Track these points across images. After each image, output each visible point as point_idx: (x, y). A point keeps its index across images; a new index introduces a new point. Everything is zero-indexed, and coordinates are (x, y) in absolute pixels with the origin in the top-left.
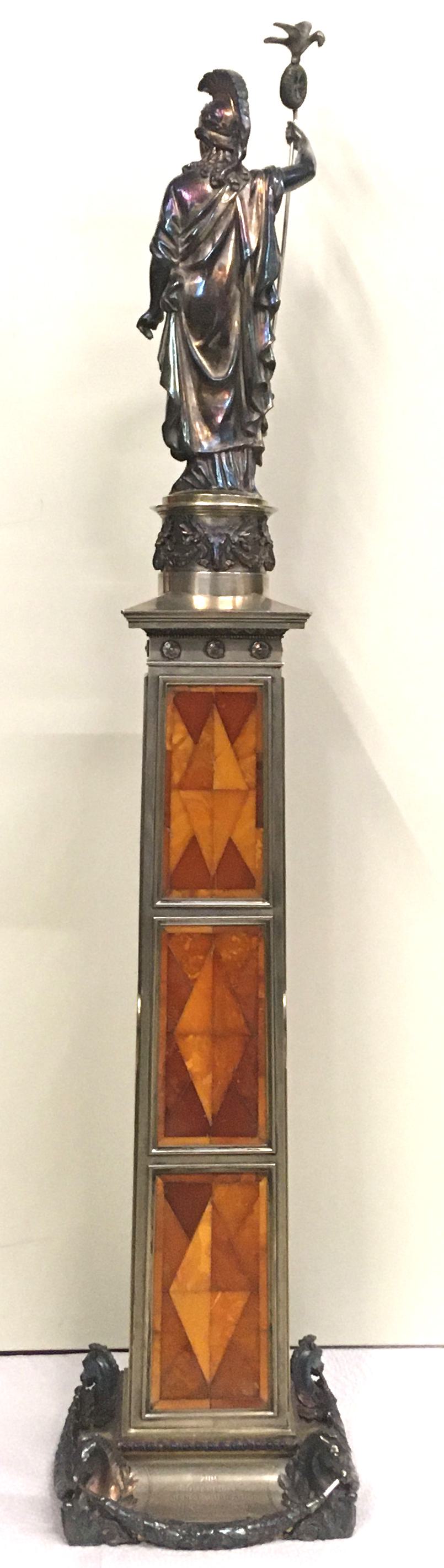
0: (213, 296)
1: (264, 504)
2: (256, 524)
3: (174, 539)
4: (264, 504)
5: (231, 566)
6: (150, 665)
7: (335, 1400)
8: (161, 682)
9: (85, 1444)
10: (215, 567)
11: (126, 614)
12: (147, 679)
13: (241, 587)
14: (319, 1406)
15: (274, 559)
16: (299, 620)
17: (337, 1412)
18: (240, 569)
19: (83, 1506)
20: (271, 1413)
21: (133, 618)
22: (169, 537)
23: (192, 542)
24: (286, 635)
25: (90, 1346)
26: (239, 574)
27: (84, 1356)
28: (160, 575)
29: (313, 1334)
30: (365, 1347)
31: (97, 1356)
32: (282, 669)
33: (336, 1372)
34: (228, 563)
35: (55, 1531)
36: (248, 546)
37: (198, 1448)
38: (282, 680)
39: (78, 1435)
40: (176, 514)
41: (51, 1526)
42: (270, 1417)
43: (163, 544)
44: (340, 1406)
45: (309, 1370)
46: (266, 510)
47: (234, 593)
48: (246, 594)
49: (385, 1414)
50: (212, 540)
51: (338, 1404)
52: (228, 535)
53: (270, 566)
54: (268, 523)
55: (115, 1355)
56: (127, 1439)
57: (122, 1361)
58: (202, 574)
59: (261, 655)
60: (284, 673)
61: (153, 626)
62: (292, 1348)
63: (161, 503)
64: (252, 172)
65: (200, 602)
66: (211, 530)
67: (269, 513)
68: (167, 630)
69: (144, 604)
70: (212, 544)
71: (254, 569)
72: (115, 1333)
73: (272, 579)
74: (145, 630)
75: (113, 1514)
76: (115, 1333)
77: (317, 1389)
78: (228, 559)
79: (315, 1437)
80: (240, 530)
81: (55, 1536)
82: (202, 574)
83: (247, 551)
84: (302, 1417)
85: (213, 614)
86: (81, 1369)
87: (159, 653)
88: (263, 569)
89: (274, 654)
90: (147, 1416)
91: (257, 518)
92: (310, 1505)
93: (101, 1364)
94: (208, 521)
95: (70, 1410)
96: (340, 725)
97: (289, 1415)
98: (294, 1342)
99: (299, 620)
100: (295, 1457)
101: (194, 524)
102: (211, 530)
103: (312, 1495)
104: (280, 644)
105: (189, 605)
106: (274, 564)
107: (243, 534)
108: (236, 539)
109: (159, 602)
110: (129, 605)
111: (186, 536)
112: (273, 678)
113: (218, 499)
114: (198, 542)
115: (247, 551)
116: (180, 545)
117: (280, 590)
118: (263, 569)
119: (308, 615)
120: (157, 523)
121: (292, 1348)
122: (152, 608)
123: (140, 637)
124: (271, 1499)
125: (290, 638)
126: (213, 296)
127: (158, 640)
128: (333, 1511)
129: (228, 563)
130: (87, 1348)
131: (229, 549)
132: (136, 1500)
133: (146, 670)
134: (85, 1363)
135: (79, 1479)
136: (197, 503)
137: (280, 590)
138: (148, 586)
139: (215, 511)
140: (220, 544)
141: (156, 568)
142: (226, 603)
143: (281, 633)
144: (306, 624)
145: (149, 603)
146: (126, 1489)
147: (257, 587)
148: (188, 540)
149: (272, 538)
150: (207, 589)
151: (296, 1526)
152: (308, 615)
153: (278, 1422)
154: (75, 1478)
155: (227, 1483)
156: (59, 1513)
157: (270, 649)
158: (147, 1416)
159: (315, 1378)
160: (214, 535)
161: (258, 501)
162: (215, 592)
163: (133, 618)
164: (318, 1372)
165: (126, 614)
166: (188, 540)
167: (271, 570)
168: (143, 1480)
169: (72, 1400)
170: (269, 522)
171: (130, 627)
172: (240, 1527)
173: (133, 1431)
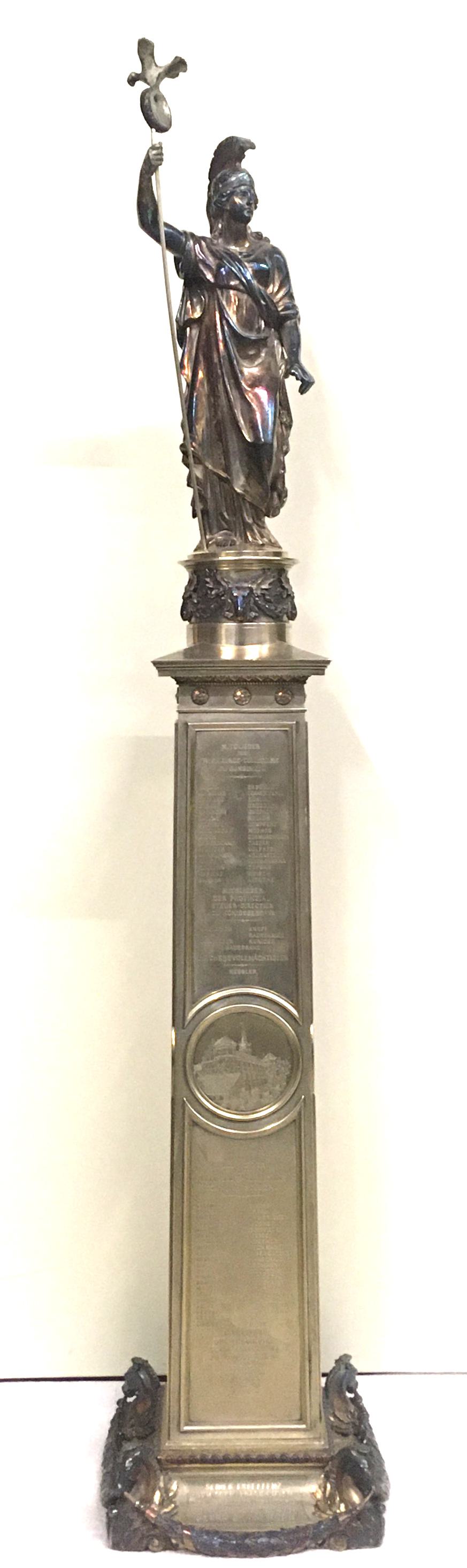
0: (234, 315)
1: (285, 556)
4: (285, 556)
5: (255, 618)
6: (180, 712)
9: (127, 1454)
10: (240, 617)
12: (176, 725)
13: (266, 636)
16: (319, 667)
18: (263, 618)
19: (127, 1522)
20: (304, 1426)
21: (162, 667)
22: (195, 590)
26: (265, 624)
28: (188, 628)
31: (139, 1370)
34: (253, 614)
36: (274, 600)
38: (306, 724)
39: (121, 1446)
40: (201, 570)
41: (101, 1532)
43: (190, 596)
45: (344, 1387)
49: (415, 1436)
51: (370, 1419)
53: (293, 616)
58: (228, 628)
60: (308, 717)
61: (180, 674)
62: (324, 1375)
64: (159, 1377)
65: (227, 651)
66: (234, 596)
67: (290, 566)
68: (194, 677)
69: (174, 654)
71: (277, 618)
74: (176, 679)
77: (352, 1408)
78: (251, 610)
79: (345, 1452)
82: (228, 628)
84: (337, 1430)
85: (239, 663)
88: (285, 618)
91: (277, 570)
93: (142, 1376)
97: (321, 1428)
98: (327, 1365)
99: (319, 667)
100: (327, 1469)
101: (219, 578)
102: (234, 596)
104: (303, 689)
105: (217, 653)
107: (263, 587)
108: (259, 592)
109: (187, 652)
110: (159, 655)
111: (212, 589)
112: (297, 723)
113: (241, 554)
115: (268, 601)
116: (206, 599)
117: (300, 638)
118: (285, 618)
119: (328, 662)
120: (184, 577)
121: (324, 1375)
122: (181, 658)
123: (170, 685)
125: (312, 684)
126: (234, 315)
127: (186, 687)
129: (253, 614)
133: (175, 717)
135: (123, 1486)
136: (220, 558)
137: (300, 638)
138: (176, 638)
140: (244, 597)
141: (184, 620)
142: (256, 652)
143: (303, 680)
144: (327, 671)
145: (178, 653)
147: (280, 635)
150: (233, 640)
152: (328, 662)
154: (120, 1486)
156: (105, 1520)
157: (293, 695)
158: (186, 1428)
159: (352, 1396)
160: (238, 588)
163: (162, 667)
164: (351, 1390)
171: (160, 675)
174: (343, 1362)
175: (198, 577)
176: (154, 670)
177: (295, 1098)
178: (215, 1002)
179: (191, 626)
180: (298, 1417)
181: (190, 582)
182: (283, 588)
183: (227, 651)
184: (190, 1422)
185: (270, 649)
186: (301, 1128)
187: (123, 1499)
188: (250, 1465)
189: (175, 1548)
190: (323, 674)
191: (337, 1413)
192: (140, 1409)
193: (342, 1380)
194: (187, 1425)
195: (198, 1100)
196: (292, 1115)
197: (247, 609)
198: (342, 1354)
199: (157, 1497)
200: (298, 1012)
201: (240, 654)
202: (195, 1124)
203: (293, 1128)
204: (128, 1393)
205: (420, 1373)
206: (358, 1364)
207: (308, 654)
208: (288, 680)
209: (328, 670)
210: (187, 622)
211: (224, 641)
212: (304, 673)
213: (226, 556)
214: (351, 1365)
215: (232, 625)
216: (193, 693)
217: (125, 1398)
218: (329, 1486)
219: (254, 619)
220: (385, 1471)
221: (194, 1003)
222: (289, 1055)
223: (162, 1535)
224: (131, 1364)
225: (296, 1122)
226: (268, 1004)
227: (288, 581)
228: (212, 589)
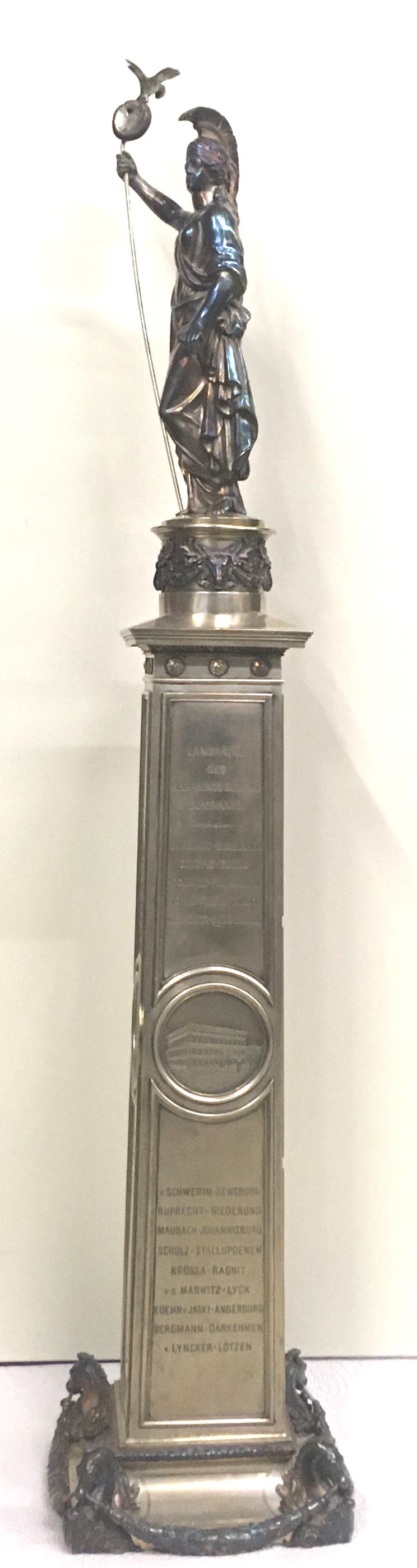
6: (155, 682)
7: (323, 1413)
10: (215, 586)
14: (308, 1418)
15: (271, 580)
16: (301, 638)
17: (326, 1423)
24: (286, 653)
25: (79, 1356)
27: (70, 1366)
29: (298, 1347)
30: (401, 1358)
32: (283, 687)
33: (320, 1384)
36: (249, 566)
37: (169, 1459)
40: (176, 536)
44: (329, 1419)
46: (264, 532)
47: (232, 611)
48: (245, 611)
50: (213, 561)
52: (230, 558)
53: (268, 587)
54: (267, 545)
55: (104, 1366)
56: (126, 1448)
57: (113, 1373)
59: (261, 674)
65: (198, 619)
68: (167, 649)
70: (214, 565)
72: (106, 1345)
73: (268, 598)
75: (118, 1523)
76: (106, 1345)
78: (230, 580)
82: (201, 597)
83: (247, 572)
86: (67, 1377)
87: (163, 668)
88: (261, 590)
89: (273, 671)
91: (254, 539)
94: (207, 543)
96: (331, 744)
97: (283, 1422)
99: (301, 638)
106: (271, 585)
115: (247, 572)
116: (180, 567)
117: (279, 608)
120: (157, 545)
123: (138, 656)
124: (267, 1505)
125: (289, 656)
129: (230, 584)
130: (76, 1359)
132: (138, 1509)
134: (72, 1371)
137: (279, 608)
138: (148, 606)
139: (215, 533)
141: (157, 589)
142: (224, 621)
143: (280, 652)
146: (128, 1496)
147: (255, 605)
149: (271, 559)
153: (272, 1428)
159: (299, 1392)
160: (217, 557)
162: (213, 610)
166: (190, 561)
167: (268, 590)
168: (155, 1489)
170: (268, 544)
172: (214, 1535)
175: (174, 544)
178: (178, 985)
180: (261, 1410)
181: (162, 551)
182: (261, 558)
183: (198, 619)
184: (149, 1418)
185: (242, 620)
186: (269, 1110)
189: (137, 1549)
190: (304, 647)
192: (86, 1408)
195: (165, 1082)
197: (226, 577)
200: (269, 990)
202: (161, 1106)
203: (260, 1112)
209: (309, 643)
210: (160, 592)
212: (284, 646)
216: (167, 662)
217: (70, 1397)
218: (294, 1483)
219: (231, 589)
220: (345, 1468)
222: (259, 1035)
223: (121, 1537)
226: (248, 987)
227: (265, 550)
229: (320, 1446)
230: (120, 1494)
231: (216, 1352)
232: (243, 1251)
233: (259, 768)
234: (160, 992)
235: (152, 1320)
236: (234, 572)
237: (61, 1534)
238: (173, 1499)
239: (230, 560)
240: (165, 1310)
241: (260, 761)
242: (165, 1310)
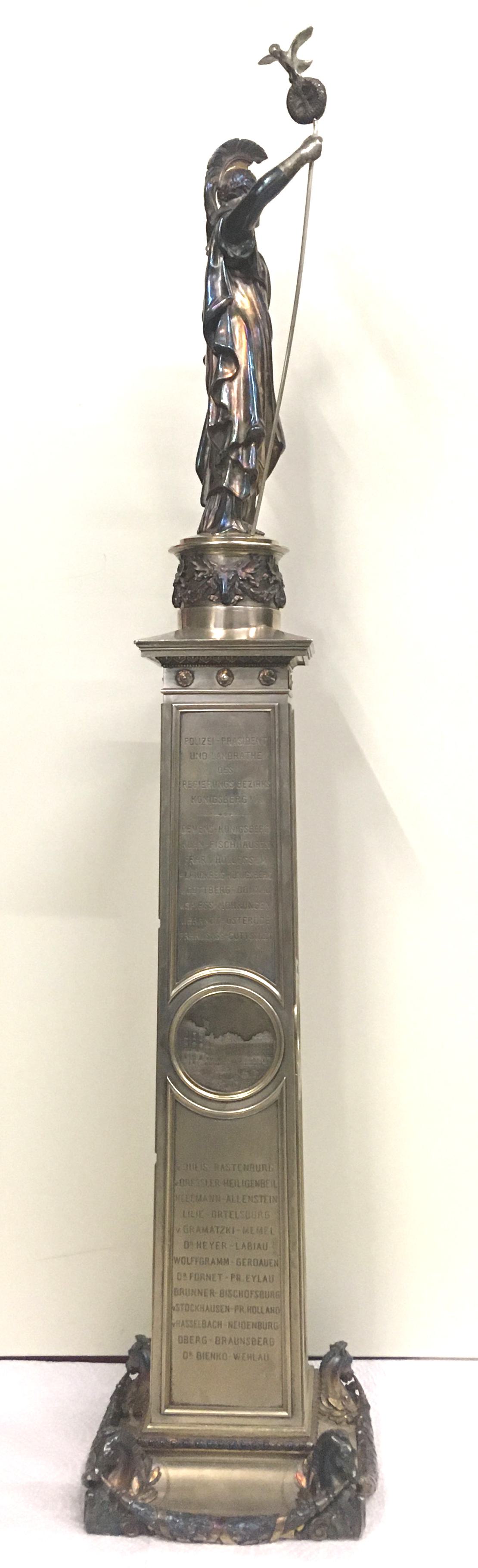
2: (263, 563)
3: (187, 577)
5: (239, 600)
8: (174, 710)
10: (225, 600)
11: (139, 644)
18: (249, 602)
20: (285, 1414)
23: (203, 577)
26: (251, 609)
34: (237, 598)
35: (76, 1519)
40: (191, 554)
41: (75, 1514)
42: (282, 1418)
47: (247, 625)
52: (235, 572)
53: (281, 604)
58: (219, 610)
63: (179, 543)
65: (217, 633)
80: (247, 567)
81: (78, 1524)
83: (254, 586)
90: (167, 1411)
91: (265, 557)
92: (319, 1504)
95: (111, 1398)
96: (348, 750)
99: (303, 646)
103: (324, 1493)
105: (208, 635)
106: (284, 602)
111: (198, 572)
114: (209, 578)
115: (254, 586)
116: (195, 582)
117: (287, 623)
120: (175, 562)
128: (343, 1513)
129: (237, 598)
131: (237, 584)
137: (287, 623)
138: (165, 621)
141: (176, 607)
142: (248, 633)
147: (267, 619)
148: (200, 575)
151: (308, 1523)
154: (97, 1470)
155: (269, 1466)
158: (167, 1411)
161: (269, 541)
165: (139, 644)
166: (200, 575)
167: (282, 607)
168: (172, 1473)
169: (114, 1388)
173: (149, 1427)
174: (339, 1349)
176: (137, 650)
177: (278, 1078)
179: (182, 611)
184: (171, 1404)
185: (256, 632)
187: (100, 1482)
188: (235, 1451)
191: (330, 1400)
193: (337, 1365)
194: (166, 1408)
196: (275, 1095)
197: (232, 590)
198: (337, 1340)
199: (135, 1484)
201: (228, 635)
204: (131, 1371)
205: (442, 1359)
206: (351, 1351)
207: (292, 635)
208: (276, 660)
211: (212, 626)
213: (216, 540)
214: (346, 1352)
215: (221, 608)
221: (178, 980)
224: (134, 1341)
225: (277, 1103)
228: (198, 572)
229: (333, 1438)
230: (139, 1478)
231: (232, 1312)
232: (250, 1326)
233: (173, 1360)
234: (174, 992)
235: (170, 1317)
236: (240, 587)
237: (83, 1525)
238: (188, 1486)
239: (236, 576)
240: (181, 1292)
241: (174, 1369)
242: (181, 1292)
